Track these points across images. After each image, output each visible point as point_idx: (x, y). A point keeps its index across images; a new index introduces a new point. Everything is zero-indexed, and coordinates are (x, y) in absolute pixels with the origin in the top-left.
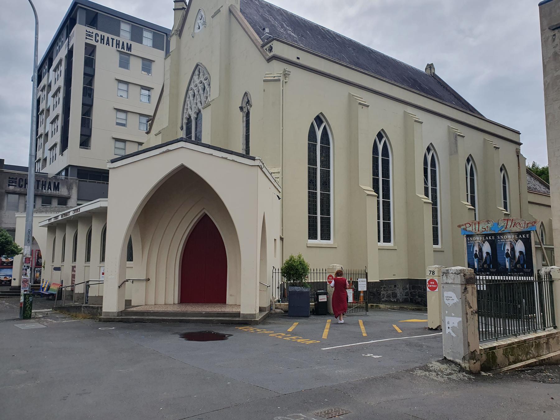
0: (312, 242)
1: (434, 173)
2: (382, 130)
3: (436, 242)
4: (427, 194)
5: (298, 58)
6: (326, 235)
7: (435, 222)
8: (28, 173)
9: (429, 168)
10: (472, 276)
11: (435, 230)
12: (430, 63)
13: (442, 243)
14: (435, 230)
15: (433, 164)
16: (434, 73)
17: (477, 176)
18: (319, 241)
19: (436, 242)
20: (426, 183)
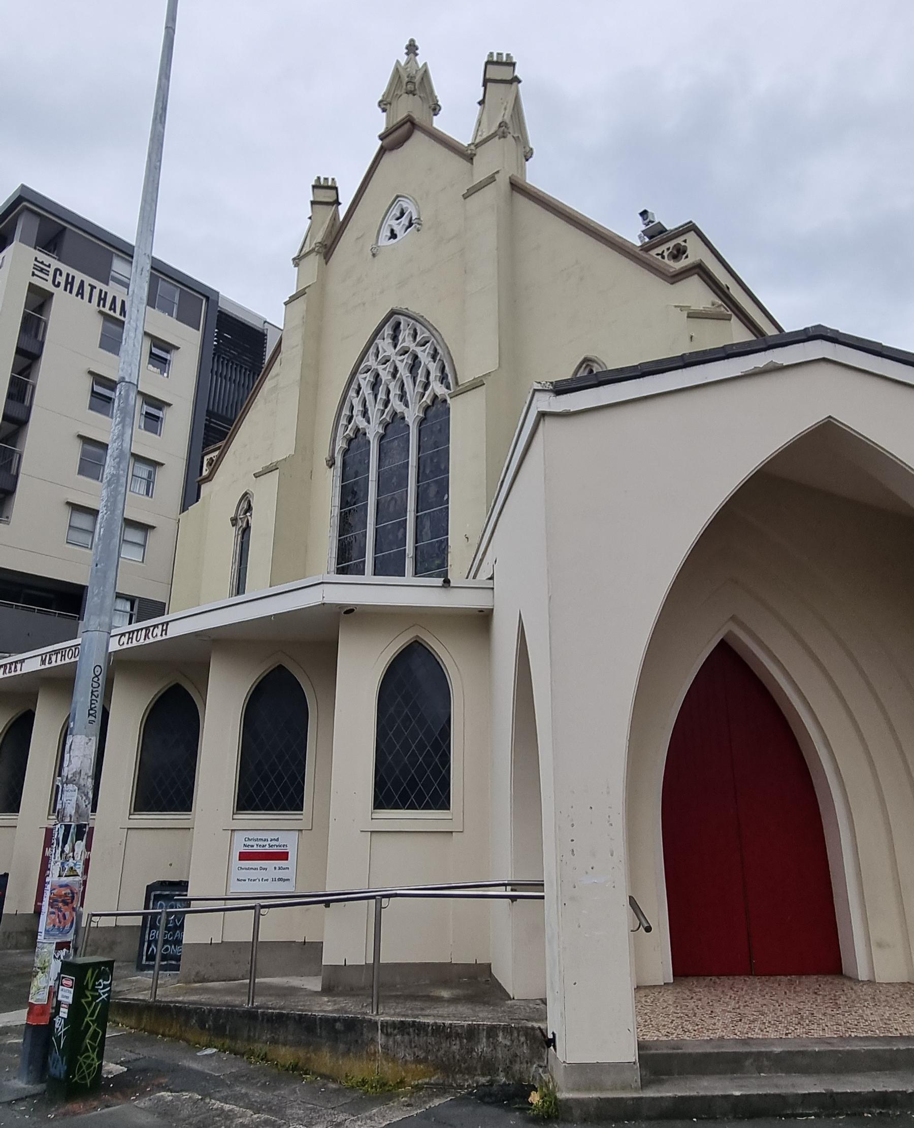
19: (284, 856)
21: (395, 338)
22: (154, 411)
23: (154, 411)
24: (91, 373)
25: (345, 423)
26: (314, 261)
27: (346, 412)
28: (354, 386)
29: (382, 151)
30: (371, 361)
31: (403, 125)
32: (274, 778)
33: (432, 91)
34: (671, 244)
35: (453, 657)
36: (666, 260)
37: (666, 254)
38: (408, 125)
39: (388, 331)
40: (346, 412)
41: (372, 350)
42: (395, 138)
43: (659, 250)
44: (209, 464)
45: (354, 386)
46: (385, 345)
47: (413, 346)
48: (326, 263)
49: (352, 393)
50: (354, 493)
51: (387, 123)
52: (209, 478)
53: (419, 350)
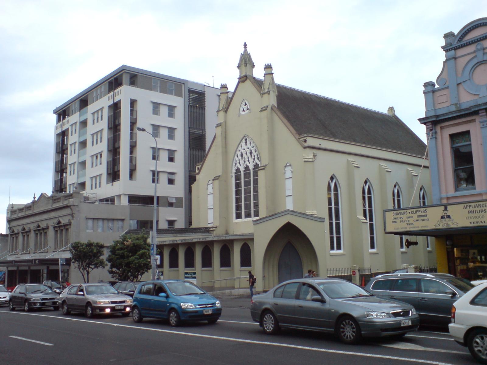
0: (332, 252)
1: (370, 198)
2: (333, 174)
3: (373, 247)
4: (365, 216)
5: (320, 144)
6: (339, 248)
7: (372, 232)
8: (334, 236)
9: (366, 196)
10: (73, 261)
11: (372, 239)
12: (391, 106)
13: (377, 247)
14: (372, 239)
15: (398, 195)
16: (394, 114)
17: (402, 194)
18: (335, 251)
19: (373, 247)
20: (364, 206)
21: (246, 142)
22: (171, 131)
23: (171, 131)
24: (152, 125)
25: (235, 165)
26: (222, 114)
27: (235, 162)
28: (236, 155)
29: (239, 83)
30: (240, 148)
31: (243, 77)
32: (226, 262)
33: (252, 61)
34: (304, 139)
35: (249, 243)
36: (303, 142)
37: (303, 141)
38: (245, 78)
39: (244, 141)
40: (235, 162)
41: (240, 145)
42: (243, 79)
43: (302, 139)
44: (198, 169)
45: (236, 155)
46: (243, 144)
47: (250, 147)
48: (226, 114)
49: (236, 157)
50: (238, 185)
51: (240, 75)
52: (199, 173)
53: (252, 149)
